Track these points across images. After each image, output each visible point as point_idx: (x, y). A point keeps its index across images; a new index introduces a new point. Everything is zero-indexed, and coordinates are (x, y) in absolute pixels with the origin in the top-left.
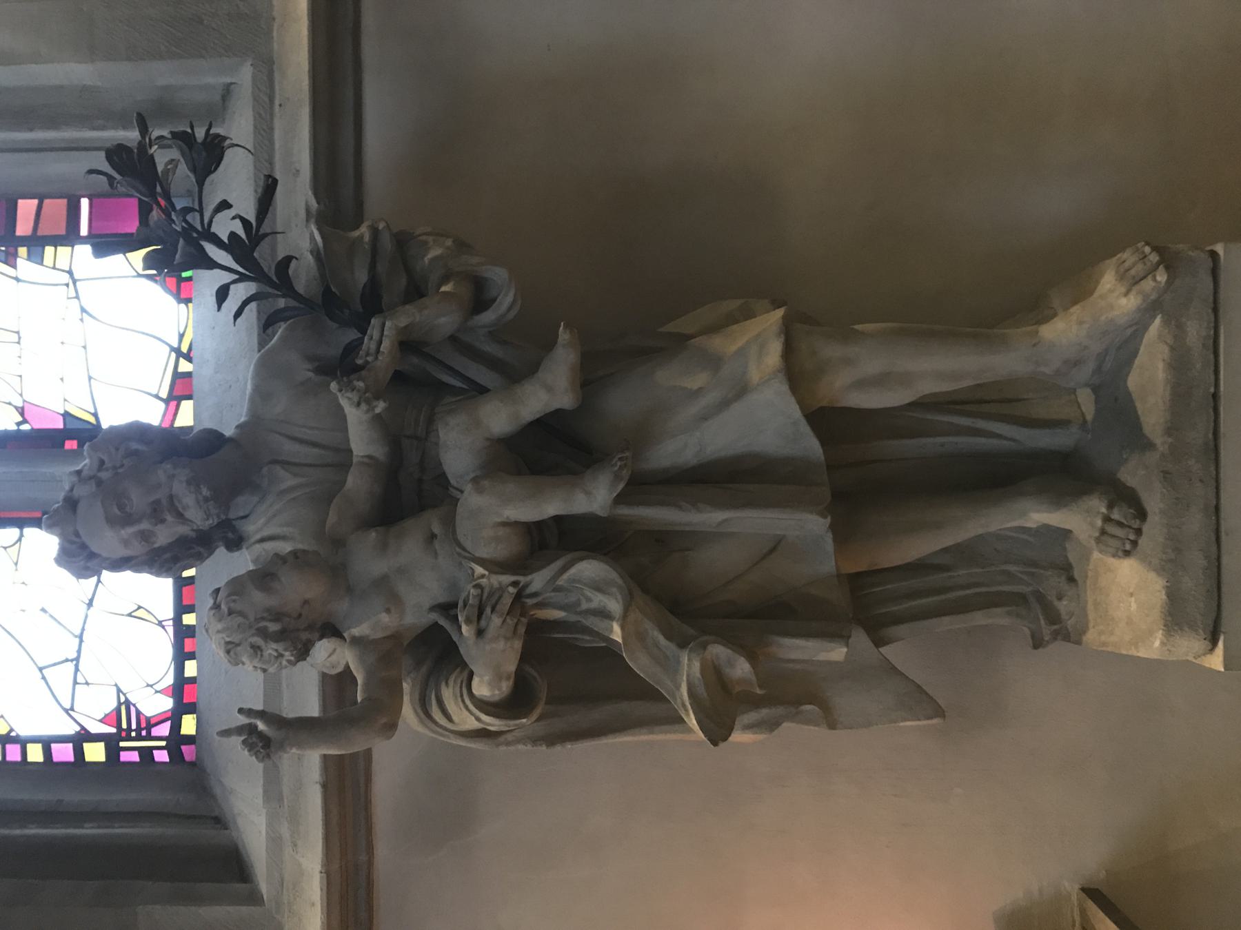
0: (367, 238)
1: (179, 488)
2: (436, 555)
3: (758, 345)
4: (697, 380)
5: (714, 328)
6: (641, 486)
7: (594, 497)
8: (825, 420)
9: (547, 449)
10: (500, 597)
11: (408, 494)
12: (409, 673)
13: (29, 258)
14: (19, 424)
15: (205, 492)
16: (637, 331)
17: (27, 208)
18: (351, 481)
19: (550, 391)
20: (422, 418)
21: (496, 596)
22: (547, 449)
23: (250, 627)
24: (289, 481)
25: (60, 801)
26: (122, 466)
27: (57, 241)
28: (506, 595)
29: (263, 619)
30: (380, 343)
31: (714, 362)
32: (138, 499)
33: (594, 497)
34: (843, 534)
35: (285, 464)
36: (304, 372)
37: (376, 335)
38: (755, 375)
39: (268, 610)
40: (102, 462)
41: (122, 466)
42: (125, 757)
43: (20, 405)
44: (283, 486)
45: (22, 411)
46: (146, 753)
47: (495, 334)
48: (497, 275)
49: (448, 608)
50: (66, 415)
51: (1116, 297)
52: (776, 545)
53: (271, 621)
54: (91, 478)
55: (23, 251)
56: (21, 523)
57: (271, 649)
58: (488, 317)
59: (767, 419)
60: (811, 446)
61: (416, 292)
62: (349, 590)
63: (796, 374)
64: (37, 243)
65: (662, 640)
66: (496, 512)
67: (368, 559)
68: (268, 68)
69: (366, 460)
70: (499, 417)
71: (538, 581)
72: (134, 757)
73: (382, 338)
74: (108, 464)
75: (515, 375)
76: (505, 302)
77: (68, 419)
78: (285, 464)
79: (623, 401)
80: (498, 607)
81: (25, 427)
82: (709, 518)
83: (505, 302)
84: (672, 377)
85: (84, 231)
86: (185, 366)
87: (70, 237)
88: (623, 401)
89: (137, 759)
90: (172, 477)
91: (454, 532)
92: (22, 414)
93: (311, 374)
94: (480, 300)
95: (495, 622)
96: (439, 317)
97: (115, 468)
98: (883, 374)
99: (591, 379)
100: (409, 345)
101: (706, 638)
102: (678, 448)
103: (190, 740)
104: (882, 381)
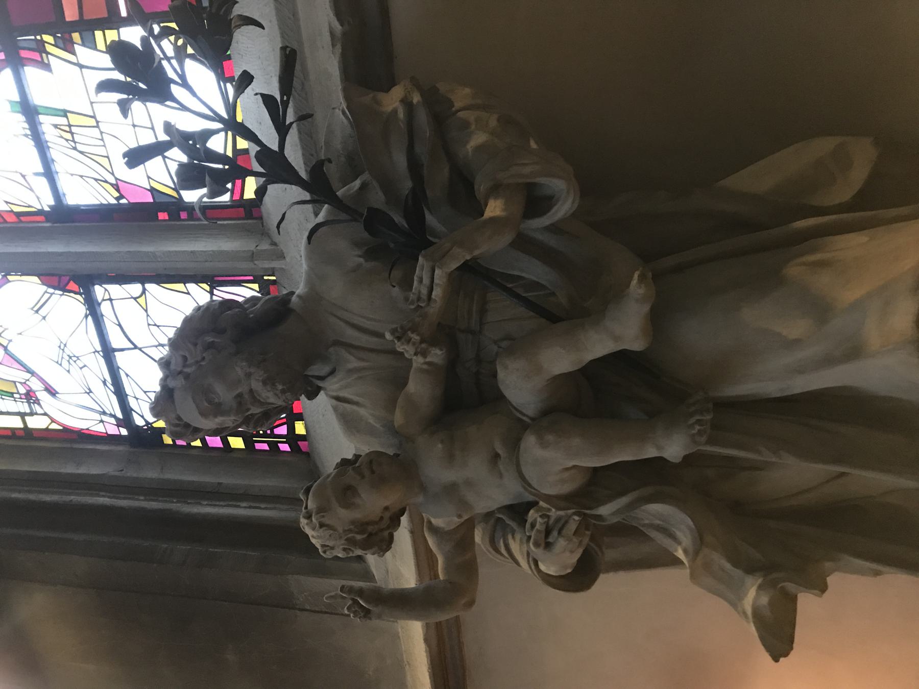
0: (401, 115)
1: (256, 385)
2: (501, 476)
4: (796, 327)
10: (566, 522)
12: (480, 522)
13: (83, 44)
14: (118, 199)
15: (280, 387)
18: (413, 386)
19: (623, 329)
20: (474, 309)
21: (562, 522)
23: (341, 538)
24: (354, 363)
25: (220, 484)
26: (203, 359)
28: (571, 521)
29: (350, 531)
30: (431, 290)
31: (820, 310)
35: (349, 346)
37: (426, 281)
38: (873, 336)
39: (353, 522)
40: (185, 358)
41: (203, 359)
42: (258, 446)
43: (114, 182)
44: (350, 366)
45: (116, 188)
46: (274, 446)
47: (554, 229)
50: (153, 190)
53: (358, 533)
54: (180, 373)
55: (76, 36)
56: (143, 279)
62: (423, 488)
65: (728, 566)
69: (425, 367)
70: (560, 359)
72: (265, 447)
74: (190, 361)
77: (154, 192)
78: (349, 346)
79: (701, 336)
80: (564, 532)
81: (123, 201)
83: (563, 209)
85: (124, 13)
88: (701, 336)
89: (268, 448)
90: (249, 375)
91: (518, 465)
92: (118, 190)
93: (361, 260)
94: (535, 202)
97: (197, 362)
101: (775, 575)
103: (302, 438)
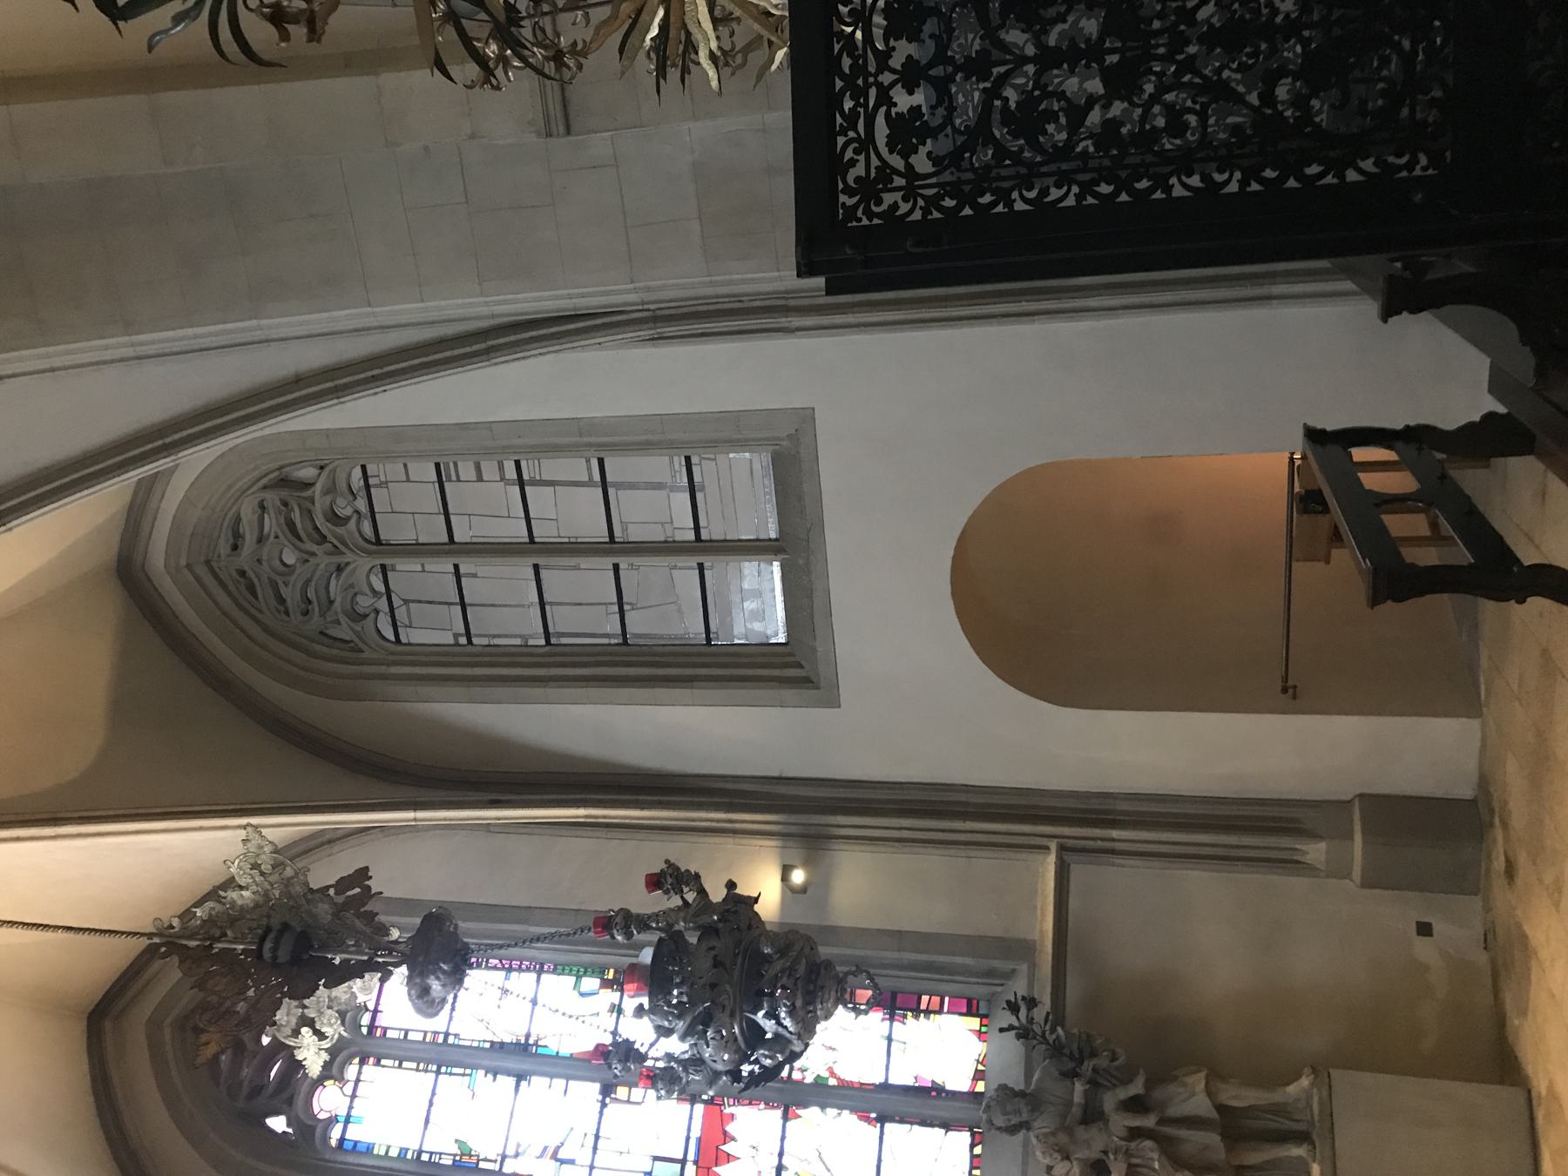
3: (1198, 1081)
4: (1181, 1090)
5: (1186, 1075)
6: (1163, 1121)
7: (1149, 1122)
8: (1221, 1109)
9: (1135, 1105)
11: (1092, 1115)
16: (1161, 1076)
17: (925, 998)
19: (1136, 1088)
22: (1135, 1105)
27: (935, 1012)
31: (1185, 1085)
32: (1009, 1108)
33: (1149, 1122)
34: (1229, 1149)
36: (1056, 1074)
47: (1117, 1069)
48: (1119, 1050)
49: (1105, 1153)
51: (1305, 1082)
52: (1207, 1147)
56: (912, 1123)
57: (1056, 1155)
58: (1116, 1063)
59: (1199, 1104)
60: (1214, 1115)
61: (1093, 1054)
63: (1209, 1093)
64: (928, 1012)
66: (1121, 1122)
67: (1081, 1132)
68: (1033, 966)
71: (1133, 1145)
73: (1088, 1066)
75: (1126, 1082)
76: (1121, 1060)
79: (1158, 1094)
82: (1183, 1133)
83: (1121, 1060)
84: (1172, 1088)
86: (981, 1067)
87: (940, 1012)
88: (1158, 1094)
95: (1120, 1156)
96: (1102, 1061)
98: (1240, 1096)
99: (1151, 1084)
100: (1094, 1070)
102: (1174, 1111)
104: (1235, 1098)
